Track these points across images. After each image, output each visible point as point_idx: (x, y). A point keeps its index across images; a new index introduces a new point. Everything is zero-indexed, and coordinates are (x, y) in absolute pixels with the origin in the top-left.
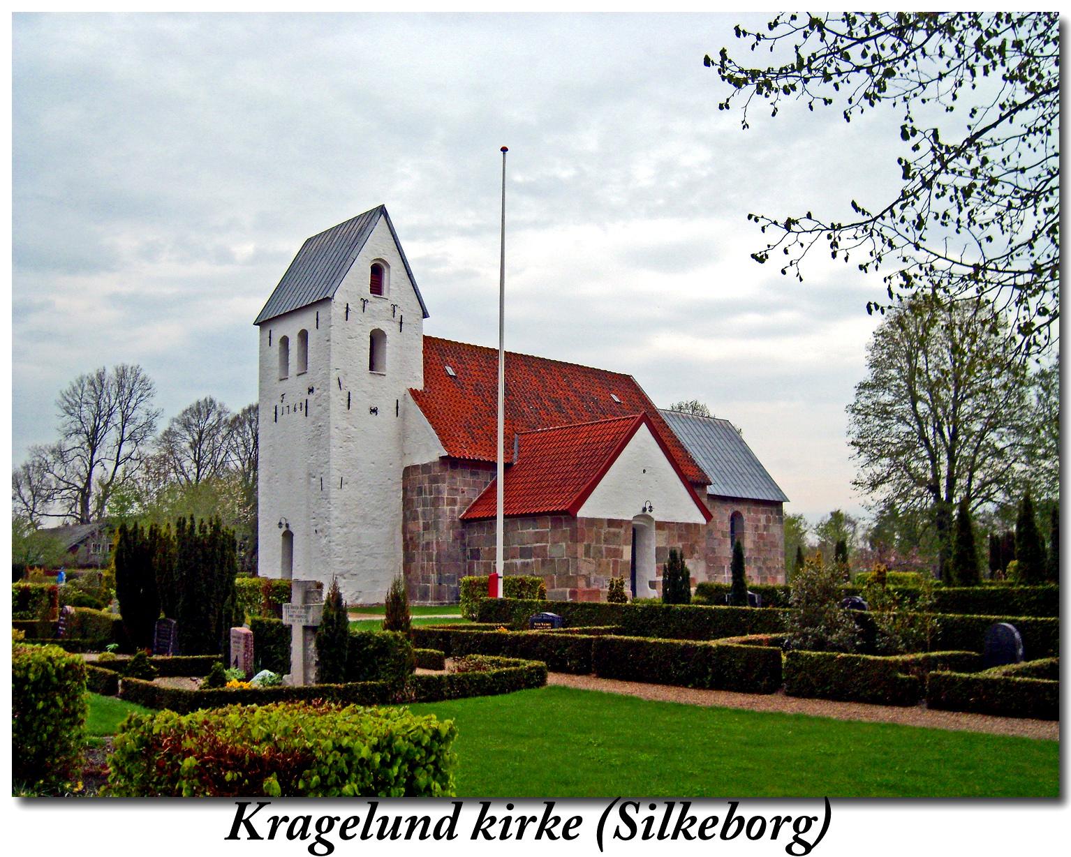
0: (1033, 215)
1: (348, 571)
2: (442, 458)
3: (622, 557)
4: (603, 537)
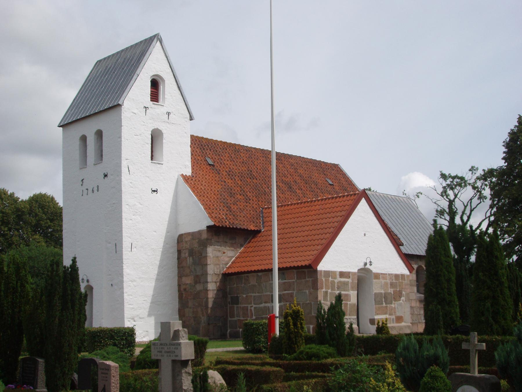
0: (81, 185)
1: (138, 316)
2: (208, 227)
3: (350, 301)
4: (336, 285)
